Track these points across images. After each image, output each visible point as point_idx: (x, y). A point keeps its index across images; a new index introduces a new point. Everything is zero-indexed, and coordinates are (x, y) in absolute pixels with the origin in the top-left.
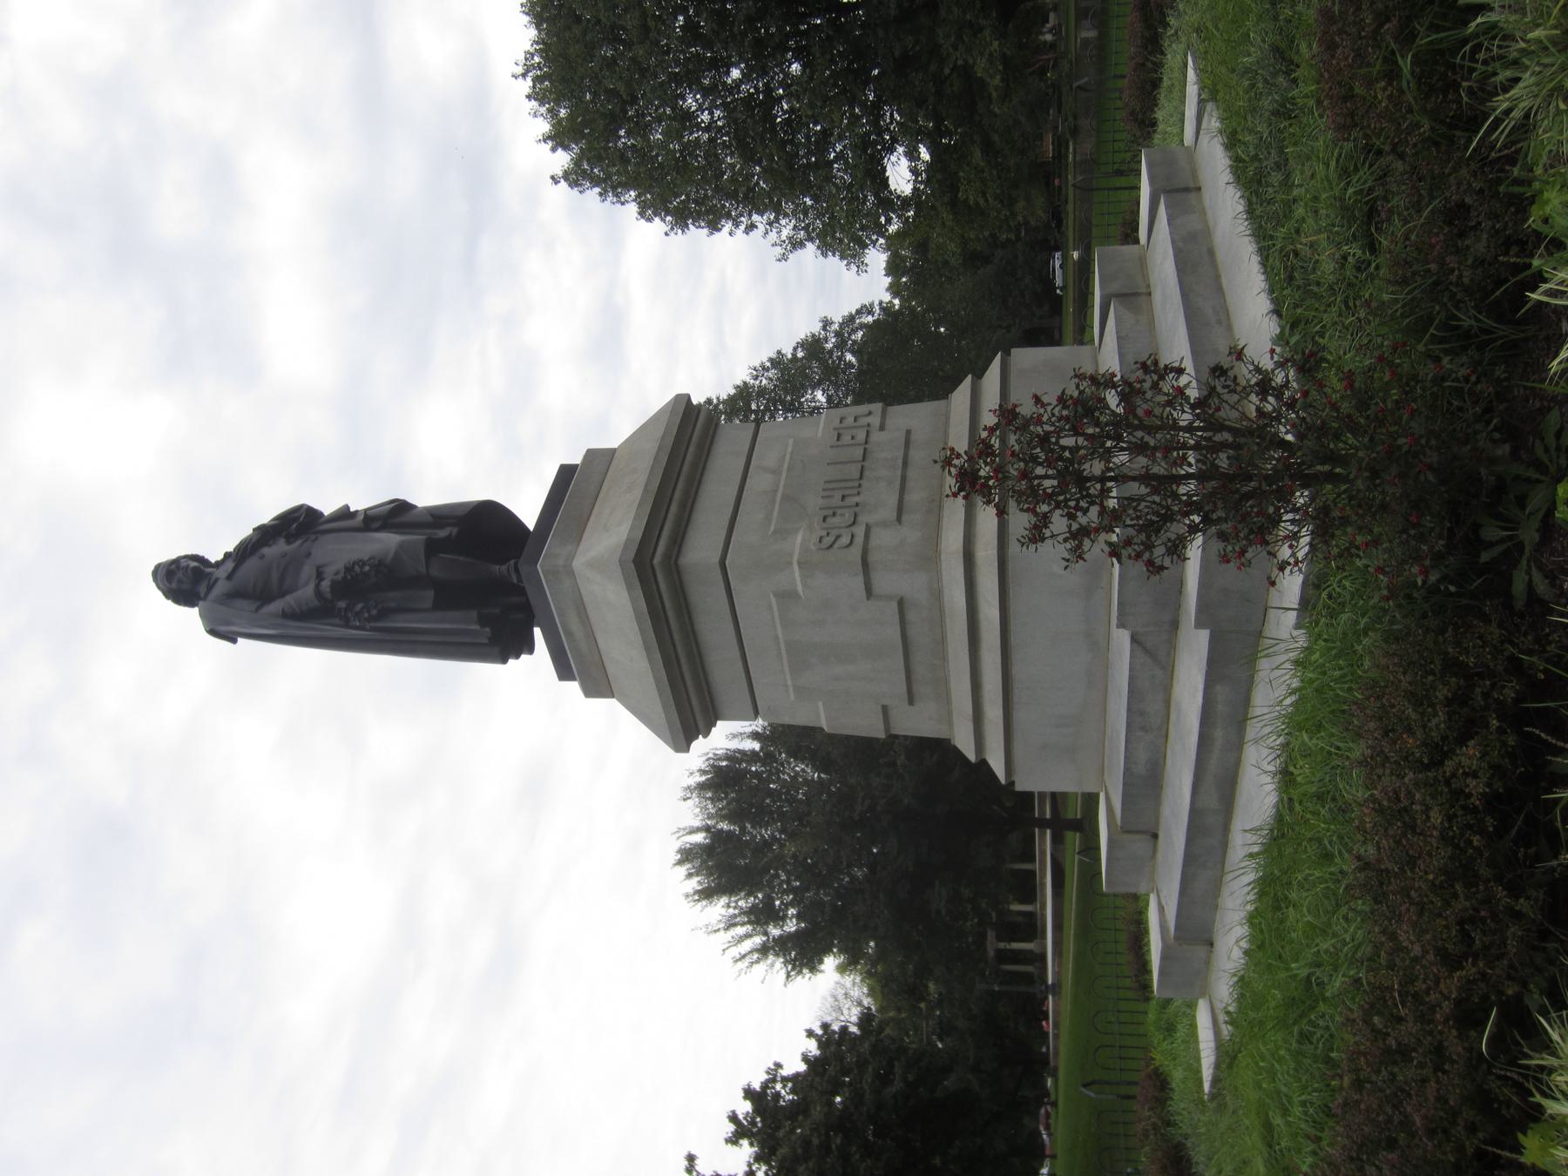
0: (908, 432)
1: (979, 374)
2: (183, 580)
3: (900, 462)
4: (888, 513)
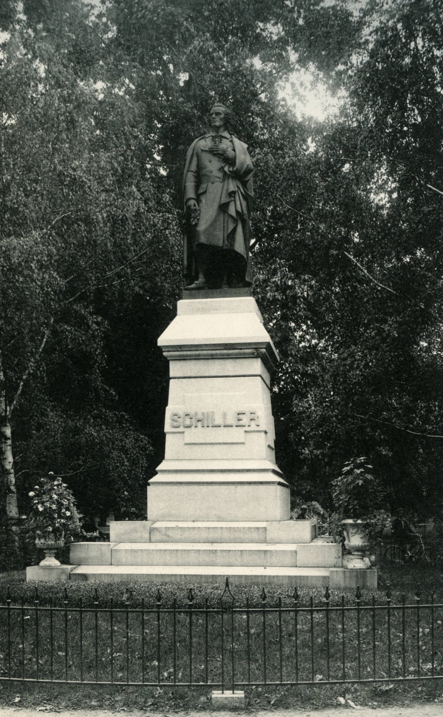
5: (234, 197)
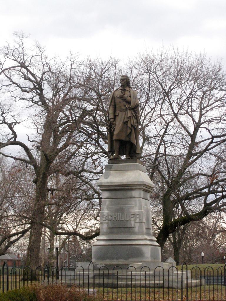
1: (157, 242)
5: (131, 118)
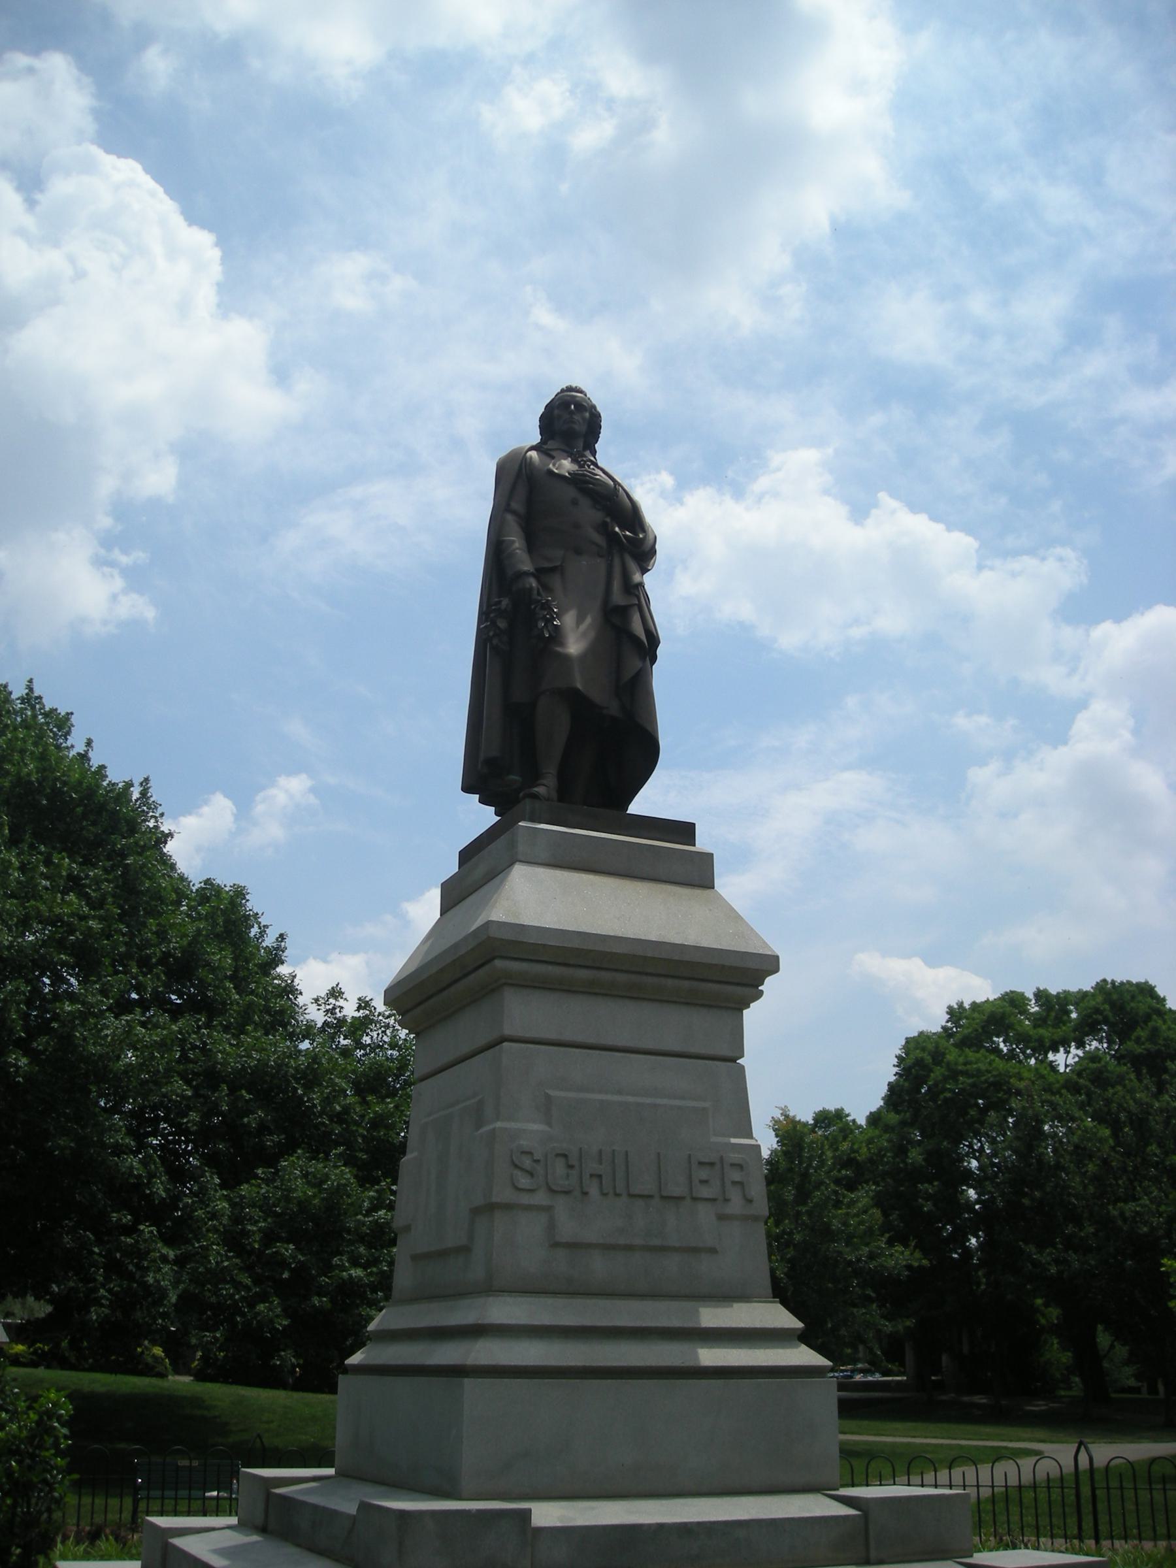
0: (713, 1251)
1: (805, 1338)
2: (570, 422)
3: (656, 1242)
4: (568, 1228)
